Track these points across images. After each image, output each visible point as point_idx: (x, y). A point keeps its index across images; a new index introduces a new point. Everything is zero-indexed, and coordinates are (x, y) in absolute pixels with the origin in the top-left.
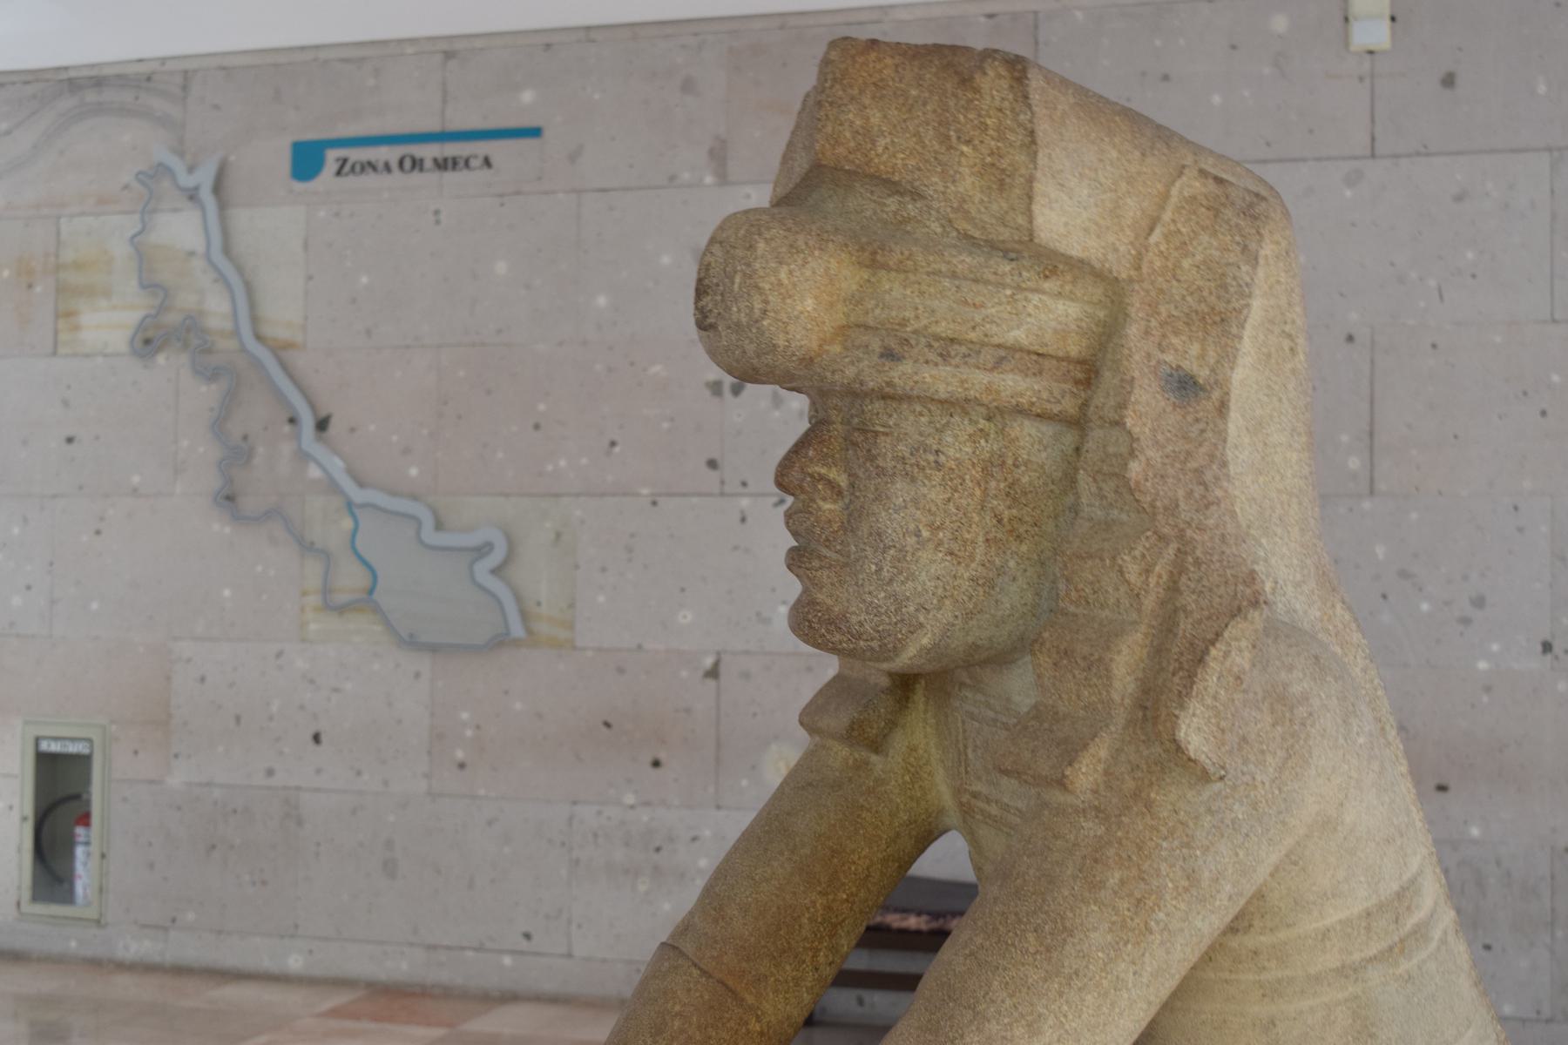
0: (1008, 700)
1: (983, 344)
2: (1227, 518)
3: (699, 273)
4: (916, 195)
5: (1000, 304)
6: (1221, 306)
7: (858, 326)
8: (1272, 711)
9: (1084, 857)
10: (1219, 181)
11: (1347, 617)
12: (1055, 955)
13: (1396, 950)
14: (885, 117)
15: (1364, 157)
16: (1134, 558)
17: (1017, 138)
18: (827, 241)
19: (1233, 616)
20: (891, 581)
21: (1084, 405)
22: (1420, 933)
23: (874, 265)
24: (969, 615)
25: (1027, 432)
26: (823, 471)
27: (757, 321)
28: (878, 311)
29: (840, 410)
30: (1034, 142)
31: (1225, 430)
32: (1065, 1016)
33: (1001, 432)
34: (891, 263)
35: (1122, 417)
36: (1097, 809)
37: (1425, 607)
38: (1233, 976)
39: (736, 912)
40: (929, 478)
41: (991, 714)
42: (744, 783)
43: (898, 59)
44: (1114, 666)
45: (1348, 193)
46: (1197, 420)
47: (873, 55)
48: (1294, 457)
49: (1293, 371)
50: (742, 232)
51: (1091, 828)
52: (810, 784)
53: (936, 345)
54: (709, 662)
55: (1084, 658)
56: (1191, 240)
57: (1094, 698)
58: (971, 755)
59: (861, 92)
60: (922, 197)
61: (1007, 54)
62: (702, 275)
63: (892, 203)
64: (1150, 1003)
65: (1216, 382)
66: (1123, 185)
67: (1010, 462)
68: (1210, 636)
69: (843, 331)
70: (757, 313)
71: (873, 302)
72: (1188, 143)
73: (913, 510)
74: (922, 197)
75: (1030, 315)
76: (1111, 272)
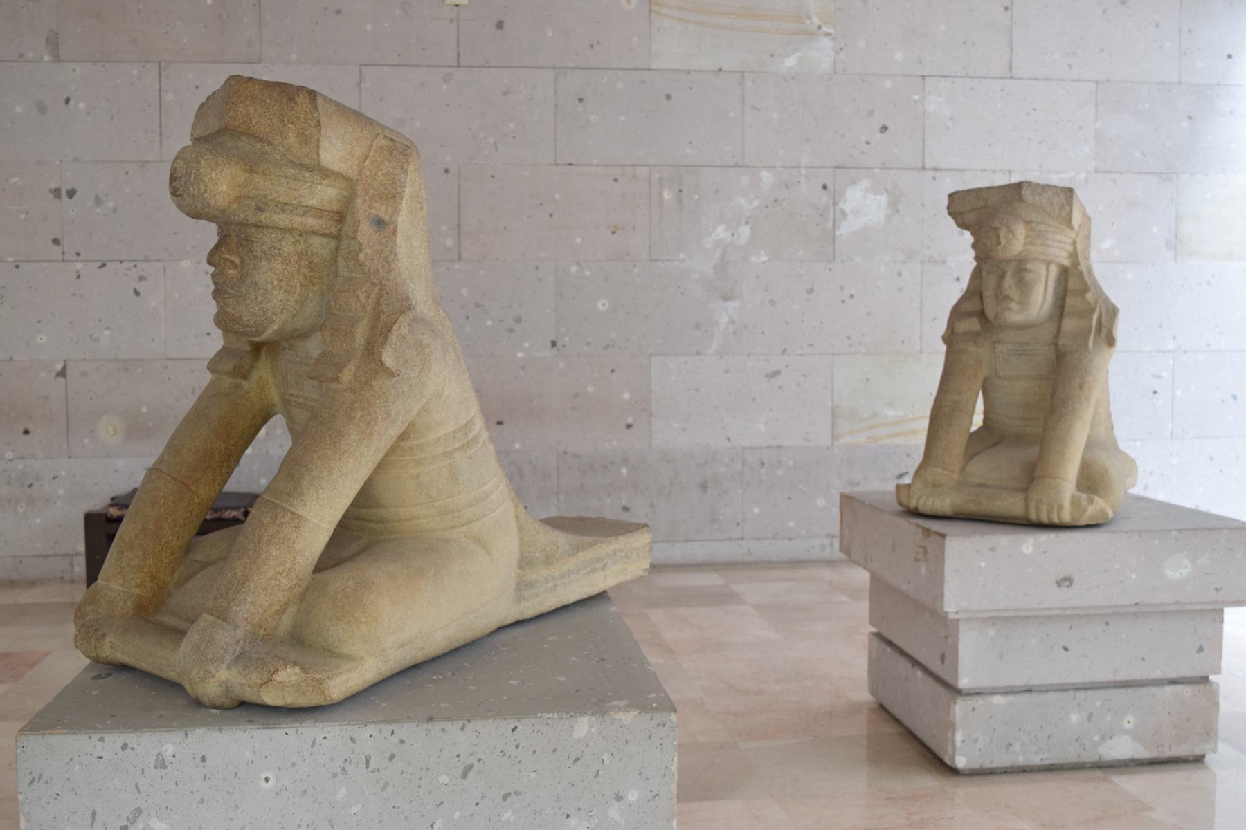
0: (307, 353)
1: (299, 206)
2: (397, 276)
3: (171, 171)
4: (270, 143)
5: (305, 189)
6: (394, 191)
7: (244, 196)
8: (417, 350)
9: (347, 408)
10: (392, 140)
11: (444, 315)
12: (337, 444)
13: (466, 446)
14: (256, 110)
15: (454, 67)
17: (313, 123)
18: (231, 161)
19: (401, 314)
20: (261, 303)
21: (340, 230)
22: (475, 440)
23: (251, 171)
24: (294, 316)
25: (316, 241)
26: (229, 257)
27: (202, 194)
28: (254, 191)
29: (235, 231)
30: (319, 125)
31: (396, 241)
32: (342, 467)
33: (306, 241)
35: (356, 236)
36: (351, 389)
37: (489, 323)
38: (403, 458)
40: (276, 260)
41: (299, 359)
42: (86, 441)
43: (261, 87)
44: (356, 334)
45: (445, 87)
46: (385, 237)
47: (250, 84)
48: (423, 251)
49: (422, 216)
50: (193, 156)
51: (349, 396)
52: (215, 395)
53: (279, 205)
54: (59, 367)
55: (344, 331)
56: (382, 164)
57: (348, 347)
58: (289, 377)
60: (272, 144)
61: (308, 89)
62: (173, 172)
63: (258, 145)
64: (373, 463)
65: (392, 221)
66: (354, 142)
67: (310, 253)
68: (393, 321)
69: (238, 199)
70: (202, 191)
71: (252, 187)
72: (379, 124)
73: (270, 273)
74: (272, 144)
75: (317, 194)
76: (349, 177)
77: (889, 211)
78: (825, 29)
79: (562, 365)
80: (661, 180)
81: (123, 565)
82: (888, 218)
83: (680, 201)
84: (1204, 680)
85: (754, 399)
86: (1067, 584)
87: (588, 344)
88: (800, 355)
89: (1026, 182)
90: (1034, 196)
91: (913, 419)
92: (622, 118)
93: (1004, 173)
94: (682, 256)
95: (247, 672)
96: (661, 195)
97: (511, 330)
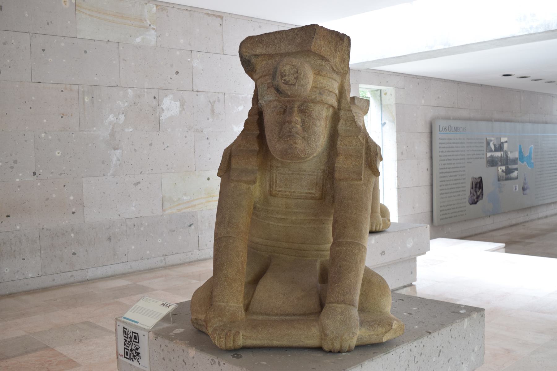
16: (360, 136)
34: (323, 74)
39: (241, 225)
59: (321, 37)
63: (319, 61)
77: (181, 109)
78: (152, 26)
79: (39, 184)
80: (83, 92)
81: (234, 291)
82: (181, 112)
83: (93, 103)
84: (411, 285)
85: (129, 196)
86: (383, 254)
87: (52, 173)
88: (148, 174)
89: (356, 97)
90: (358, 102)
91: (194, 200)
92: (64, 61)
93: (222, 94)
94: (95, 129)
95: (373, 328)
96: (84, 99)
97: (12, 167)
